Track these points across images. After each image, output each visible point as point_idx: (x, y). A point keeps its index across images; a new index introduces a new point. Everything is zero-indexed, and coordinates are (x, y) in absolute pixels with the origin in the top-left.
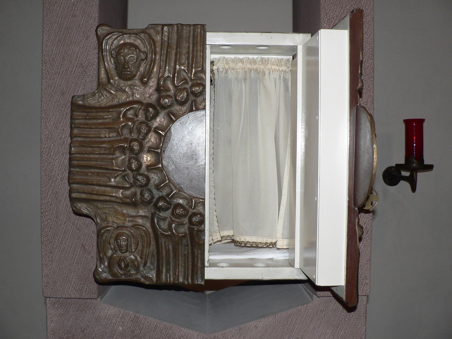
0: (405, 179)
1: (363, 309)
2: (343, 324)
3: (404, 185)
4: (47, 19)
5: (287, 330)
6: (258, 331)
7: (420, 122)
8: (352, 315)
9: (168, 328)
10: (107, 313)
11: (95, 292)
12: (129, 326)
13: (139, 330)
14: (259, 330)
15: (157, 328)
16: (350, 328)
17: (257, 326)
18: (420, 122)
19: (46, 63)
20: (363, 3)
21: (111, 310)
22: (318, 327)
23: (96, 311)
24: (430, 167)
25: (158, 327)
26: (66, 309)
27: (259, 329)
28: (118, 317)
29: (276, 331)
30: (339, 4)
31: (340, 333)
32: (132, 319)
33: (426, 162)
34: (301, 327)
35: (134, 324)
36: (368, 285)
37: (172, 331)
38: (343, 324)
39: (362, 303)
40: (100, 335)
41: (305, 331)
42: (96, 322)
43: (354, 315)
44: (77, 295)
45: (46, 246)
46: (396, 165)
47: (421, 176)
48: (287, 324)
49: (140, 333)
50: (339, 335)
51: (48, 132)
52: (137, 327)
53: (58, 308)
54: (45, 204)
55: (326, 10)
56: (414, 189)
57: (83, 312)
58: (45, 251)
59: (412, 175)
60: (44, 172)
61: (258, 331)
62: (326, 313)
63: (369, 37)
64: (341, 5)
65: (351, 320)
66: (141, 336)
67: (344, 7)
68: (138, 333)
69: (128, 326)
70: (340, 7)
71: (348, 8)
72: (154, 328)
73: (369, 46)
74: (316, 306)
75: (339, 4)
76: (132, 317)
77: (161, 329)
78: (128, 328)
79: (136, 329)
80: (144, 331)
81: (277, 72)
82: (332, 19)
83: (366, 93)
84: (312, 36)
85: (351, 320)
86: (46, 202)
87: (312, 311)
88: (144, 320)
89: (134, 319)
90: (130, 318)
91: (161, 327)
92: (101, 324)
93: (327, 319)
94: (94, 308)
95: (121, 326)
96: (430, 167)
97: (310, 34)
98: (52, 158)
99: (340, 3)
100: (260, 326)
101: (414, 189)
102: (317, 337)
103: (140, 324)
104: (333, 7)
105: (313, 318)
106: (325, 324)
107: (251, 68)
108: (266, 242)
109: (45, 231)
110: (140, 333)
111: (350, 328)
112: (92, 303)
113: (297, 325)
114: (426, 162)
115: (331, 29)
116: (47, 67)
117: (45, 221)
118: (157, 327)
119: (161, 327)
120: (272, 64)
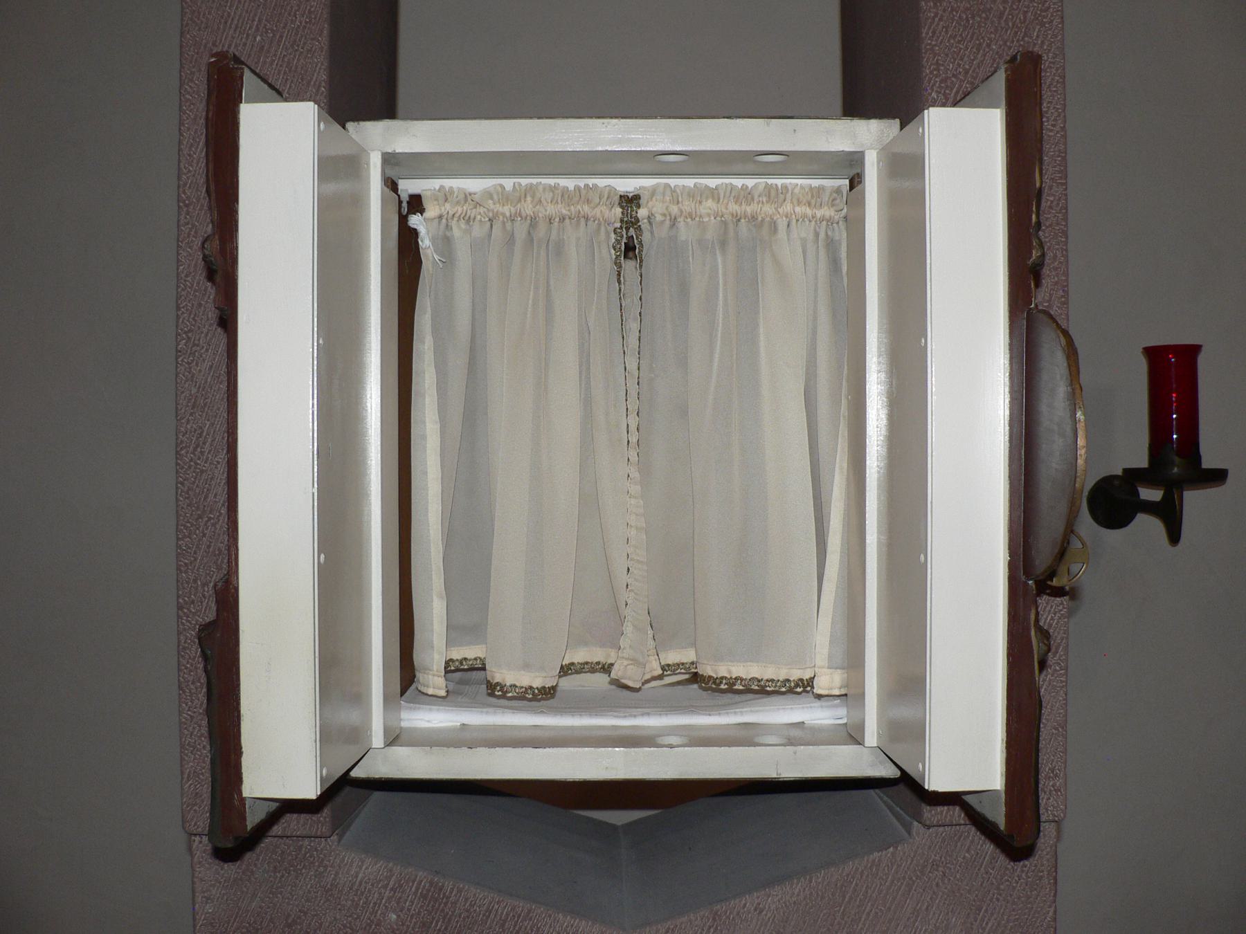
10: (357, 877)
13: (443, 922)
27: (766, 915)
31: (987, 924)
32: (424, 892)
43: (1024, 875)
76: (424, 886)
85: (1014, 888)
88: (455, 895)
89: (428, 891)
90: (417, 889)
91: (502, 913)
112: (316, 850)
119: (502, 913)
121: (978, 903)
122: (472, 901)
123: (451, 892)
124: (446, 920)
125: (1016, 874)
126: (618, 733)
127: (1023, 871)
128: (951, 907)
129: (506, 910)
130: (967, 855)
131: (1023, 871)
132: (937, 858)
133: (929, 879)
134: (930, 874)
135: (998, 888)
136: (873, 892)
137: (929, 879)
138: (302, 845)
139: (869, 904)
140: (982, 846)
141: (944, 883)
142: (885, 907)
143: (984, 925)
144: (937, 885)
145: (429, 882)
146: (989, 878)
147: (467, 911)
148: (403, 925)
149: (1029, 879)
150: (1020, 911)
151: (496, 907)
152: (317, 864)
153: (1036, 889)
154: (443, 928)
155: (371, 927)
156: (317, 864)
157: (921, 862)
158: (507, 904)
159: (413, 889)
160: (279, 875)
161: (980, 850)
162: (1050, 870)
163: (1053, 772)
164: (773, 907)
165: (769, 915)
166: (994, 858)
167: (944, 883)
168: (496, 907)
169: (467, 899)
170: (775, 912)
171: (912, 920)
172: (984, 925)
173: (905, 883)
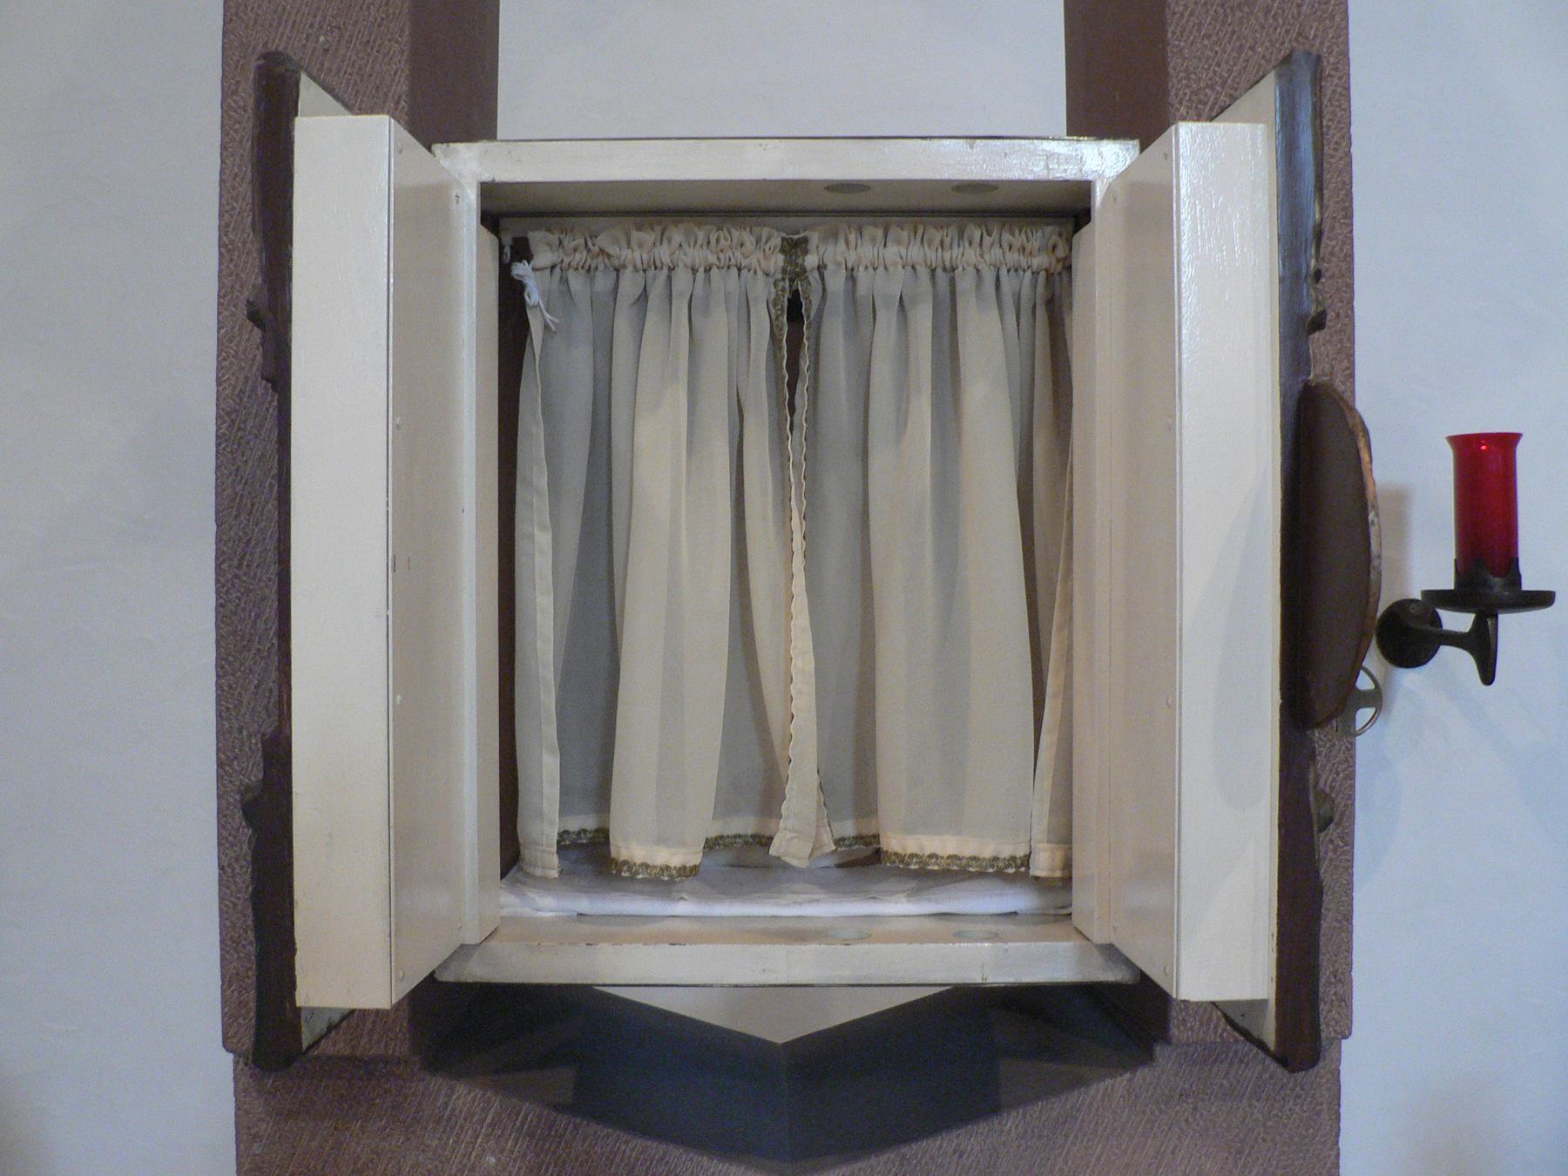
0: (1455, 640)
1: (1329, 1089)
2: (1260, 1140)
3: (1456, 662)
4: (235, 101)
5: (1066, 1163)
7: (1506, 443)
8: (1290, 1110)
9: (653, 1158)
11: (404, 1034)
12: (519, 1152)
14: (970, 1162)
15: (617, 1160)
18: (1506, 443)
19: (234, 249)
20: (1312, 32)
21: (458, 1098)
22: (1173, 1153)
24: (1543, 599)
29: (1027, 1167)
30: (1231, 38)
33: (1529, 583)
36: (1343, 1004)
37: (667, 1168)
38: (1260, 1140)
42: (408, 1139)
43: (1297, 1109)
44: (342, 1045)
45: (234, 877)
46: (1426, 593)
47: (1510, 625)
48: (1066, 1141)
51: (241, 487)
54: (230, 733)
55: (1184, 58)
56: (1488, 675)
58: (232, 896)
59: (1479, 625)
60: (229, 625)
63: (1336, 150)
64: (1238, 44)
65: (1285, 1125)
67: (1246, 48)
70: (1233, 50)
71: (1260, 53)
73: (1333, 181)
75: (1231, 38)
76: (532, 1121)
81: (1022, 273)
82: (1207, 90)
83: (1328, 341)
84: (1142, 149)
85: (1285, 1125)
86: (236, 725)
90: (523, 1124)
92: (422, 1146)
93: (1201, 1123)
95: (493, 1154)
96: (1543, 599)
97: (1136, 142)
98: (255, 574)
99: (1235, 37)
101: (1488, 675)
104: (1212, 50)
107: (934, 261)
108: (994, 854)
109: (233, 827)
113: (1098, 1142)
114: (1529, 583)
115: (352, 1012)
116: (236, 266)
117: (233, 791)
118: (615, 1156)
119: (630, 1156)
120: (1006, 248)
121: (1239, 1145)
132: (1187, 1086)
135: (1264, 1125)
139: (1100, 1145)
147: (587, 1153)
149: (1305, 1115)
151: (623, 1147)
159: (518, 1123)
165: (972, 1158)
168: (623, 1147)
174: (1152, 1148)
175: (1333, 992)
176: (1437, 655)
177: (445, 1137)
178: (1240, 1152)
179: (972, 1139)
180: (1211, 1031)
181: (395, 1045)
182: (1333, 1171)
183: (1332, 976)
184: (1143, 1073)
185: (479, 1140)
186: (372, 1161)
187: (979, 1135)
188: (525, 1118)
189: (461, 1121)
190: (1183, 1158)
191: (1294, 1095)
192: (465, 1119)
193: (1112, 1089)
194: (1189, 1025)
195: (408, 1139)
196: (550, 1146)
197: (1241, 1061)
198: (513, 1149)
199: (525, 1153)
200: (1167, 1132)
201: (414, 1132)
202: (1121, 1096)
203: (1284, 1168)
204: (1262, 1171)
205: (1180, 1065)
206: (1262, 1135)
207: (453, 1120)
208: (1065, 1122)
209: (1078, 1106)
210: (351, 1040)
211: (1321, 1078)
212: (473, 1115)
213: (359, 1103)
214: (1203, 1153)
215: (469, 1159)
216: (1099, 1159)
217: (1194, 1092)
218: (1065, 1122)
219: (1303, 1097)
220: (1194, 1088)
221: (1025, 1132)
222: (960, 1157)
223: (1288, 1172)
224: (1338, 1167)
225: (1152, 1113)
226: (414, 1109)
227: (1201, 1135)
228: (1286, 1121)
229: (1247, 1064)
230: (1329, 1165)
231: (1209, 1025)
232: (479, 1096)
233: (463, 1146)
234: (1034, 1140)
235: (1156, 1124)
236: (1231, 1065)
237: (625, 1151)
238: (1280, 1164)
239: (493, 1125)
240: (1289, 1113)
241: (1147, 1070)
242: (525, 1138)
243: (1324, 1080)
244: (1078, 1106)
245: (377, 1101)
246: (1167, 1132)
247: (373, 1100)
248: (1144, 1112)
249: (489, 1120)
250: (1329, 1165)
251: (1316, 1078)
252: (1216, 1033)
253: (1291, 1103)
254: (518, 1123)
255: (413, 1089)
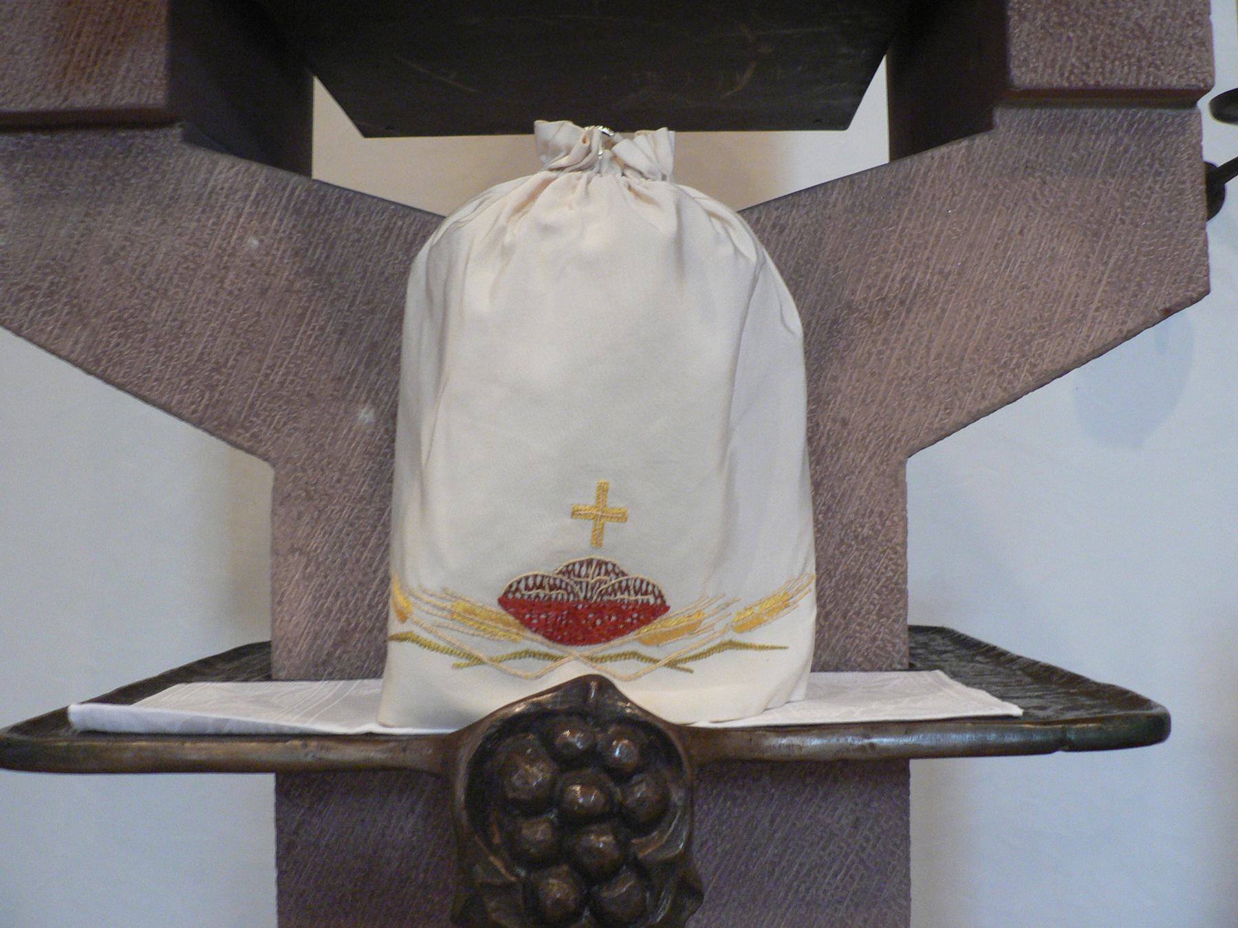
5: (901, 243)
6: (785, 242)
10: (205, 185)
13: (323, 248)
14: (792, 238)
16: (1146, 237)
17: (782, 221)
21: (221, 173)
22: (1021, 232)
23: (163, 178)
25: (396, 232)
26: (52, 178)
27: (789, 235)
28: (246, 198)
31: (1110, 257)
32: (299, 205)
34: (954, 232)
35: (303, 224)
38: (1118, 222)
39: (1184, 142)
40: (175, 273)
41: (971, 246)
42: (164, 222)
43: (1157, 187)
49: (327, 257)
50: (1106, 264)
52: (313, 236)
53: (27, 174)
57: (117, 184)
61: (785, 242)
62: (1048, 177)
65: (1145, 205)
66: (329, 269)
68: (318, 259)
69: (281, 235)
72: (382, 236)
74: (1007, 147)
76: (299, 196)
77: (406, 239)
78: (281, 239)
79: (310, 243)
80: (340, 252)
85: (1145, 205)
87: (994, 165)
88: (343, 208)
89: (304, 202)
90: (289, 201)
91: (407, 233)
93: (1052, 200)
94: (158, 168)
100: (794, 224)
102: (1020, 272)
103: (327, 225)
105: (1001, 194)
106: (1049, 219)
110: (327, 257)
111: (1146, 237)
112: (151, 150)
119: (407, 233)
121: (1095, 226)
122: (365, 216)
123: (336, 204)
124: (328, 246)
125: (1147, 185)
126: (649, 719)
127: (1155, 182)
128: (1057, 231)
129: (413, 228)
130: (1074, 155)
131: (1155, 182)
132: (1033, 157)
133: (1023, 188)
134: (1024, 182)
135: (1122, 205)
136: (943, 204)
137: (1023, 188)
138: (131, 145)
139: (939, 223)
140: (1095, 143)
141: (1043, 195)
142: (961, 228)
143: (1105, 259)
144: (1035, 199)
145: (306, 190)
146: (1109, 190)
147: (358, 230)
148: (268, 254)
149: (1167, 194)
150: (1155, 240)
151: (400, 223)
152: (151, 170)
153: (1176, 208)
154: (324, 256)
155: (222, 257)
156: (151, 170)
157: (1010, 162)
158: (415, 219)
159: (284, 200)
160: (99, 188)
161: (1092, 148)
162: (1195, 181)
163: (1192, 18)
164: (799, 223)
165: (794, 234)
166: (1114, 161)
167: (1043, 195)
168: (400, 223)
169: (357, 214)
170: (803, 231)
171: (1002, 248)
172: (1105, 259)
173: (988, 193)
174: (997, 227)
175: (1191, 35)
176: (1221, 211)
177: (203, 219)
178: (1096, 234)
179: (794, 211)
180: (1057, 75)
181: (149, 94)
182: (1202, 259)
183: (1188, 18)
184: (980, 141)
185: (242, 220)
186: (123, 248)
187: (801, 208)
188: (292, 194)
189: (222, 199)
190: (1033, 239)
191: (1154, 171)
192: (227, 197)
193: (949, 158)
194: (1031, 66)
195: (164, 222)
196: (319, 225)
197: (1092, 132)
198: (278, 228)
199: (291, 233)
200: (1013, 209)
201: (170, 215)
202: (959, 167)
203: (1148, 254)
204: (1122, 258)
205: (1023, 134)
206: (1119, 216)
207: (214, 197)
208: (897, 194)
209: (911, 176)
210: (103, 89)
211: (1182, 153)
212: (237, 191)
213: (113, 185)
214: (1056, 234)
215: (229, 243)
216: (938, 237)
217: (1041, 165)
218: (897, 194)
219: (1163, 175)
220: (1041, 160)
221: (854, 204)
222: (782, 231)
223: (1151, 259)
224: (1206, 254)
225: (996, 187)
226: (172, 187)
227: (1052, 214)
228: (1146, 201)
229: (1098, 134)
230: (1197, 252)
231: (1053, 67)
232: (243, 169)
233: (224, 227)
234: (864, 214)
235: (1001, 200)
236: (1081, 134)
237: (401, 228)
238: (1143, 249)
239: (256, 203)
240: (1148, 192)
241: (986, 137)
242: (292, 214)
243: (1185, 156)
244: (911, 176)
245: (133, 181)
246: (1013, 209)
247: (128, 179)
248: (986, 185)
249: (252, 198)
250: (1197, 252)
251: (1175, 154)
252: (1062, 75)
253: (1150, 180)
254: (284, 200)
255: (172, 165)
